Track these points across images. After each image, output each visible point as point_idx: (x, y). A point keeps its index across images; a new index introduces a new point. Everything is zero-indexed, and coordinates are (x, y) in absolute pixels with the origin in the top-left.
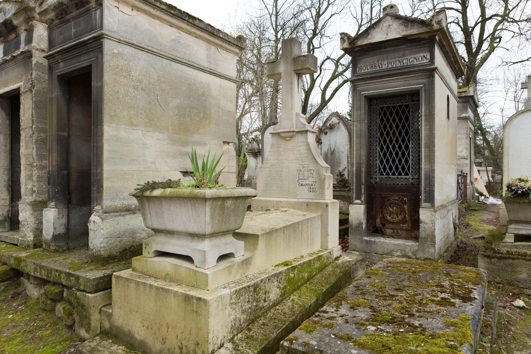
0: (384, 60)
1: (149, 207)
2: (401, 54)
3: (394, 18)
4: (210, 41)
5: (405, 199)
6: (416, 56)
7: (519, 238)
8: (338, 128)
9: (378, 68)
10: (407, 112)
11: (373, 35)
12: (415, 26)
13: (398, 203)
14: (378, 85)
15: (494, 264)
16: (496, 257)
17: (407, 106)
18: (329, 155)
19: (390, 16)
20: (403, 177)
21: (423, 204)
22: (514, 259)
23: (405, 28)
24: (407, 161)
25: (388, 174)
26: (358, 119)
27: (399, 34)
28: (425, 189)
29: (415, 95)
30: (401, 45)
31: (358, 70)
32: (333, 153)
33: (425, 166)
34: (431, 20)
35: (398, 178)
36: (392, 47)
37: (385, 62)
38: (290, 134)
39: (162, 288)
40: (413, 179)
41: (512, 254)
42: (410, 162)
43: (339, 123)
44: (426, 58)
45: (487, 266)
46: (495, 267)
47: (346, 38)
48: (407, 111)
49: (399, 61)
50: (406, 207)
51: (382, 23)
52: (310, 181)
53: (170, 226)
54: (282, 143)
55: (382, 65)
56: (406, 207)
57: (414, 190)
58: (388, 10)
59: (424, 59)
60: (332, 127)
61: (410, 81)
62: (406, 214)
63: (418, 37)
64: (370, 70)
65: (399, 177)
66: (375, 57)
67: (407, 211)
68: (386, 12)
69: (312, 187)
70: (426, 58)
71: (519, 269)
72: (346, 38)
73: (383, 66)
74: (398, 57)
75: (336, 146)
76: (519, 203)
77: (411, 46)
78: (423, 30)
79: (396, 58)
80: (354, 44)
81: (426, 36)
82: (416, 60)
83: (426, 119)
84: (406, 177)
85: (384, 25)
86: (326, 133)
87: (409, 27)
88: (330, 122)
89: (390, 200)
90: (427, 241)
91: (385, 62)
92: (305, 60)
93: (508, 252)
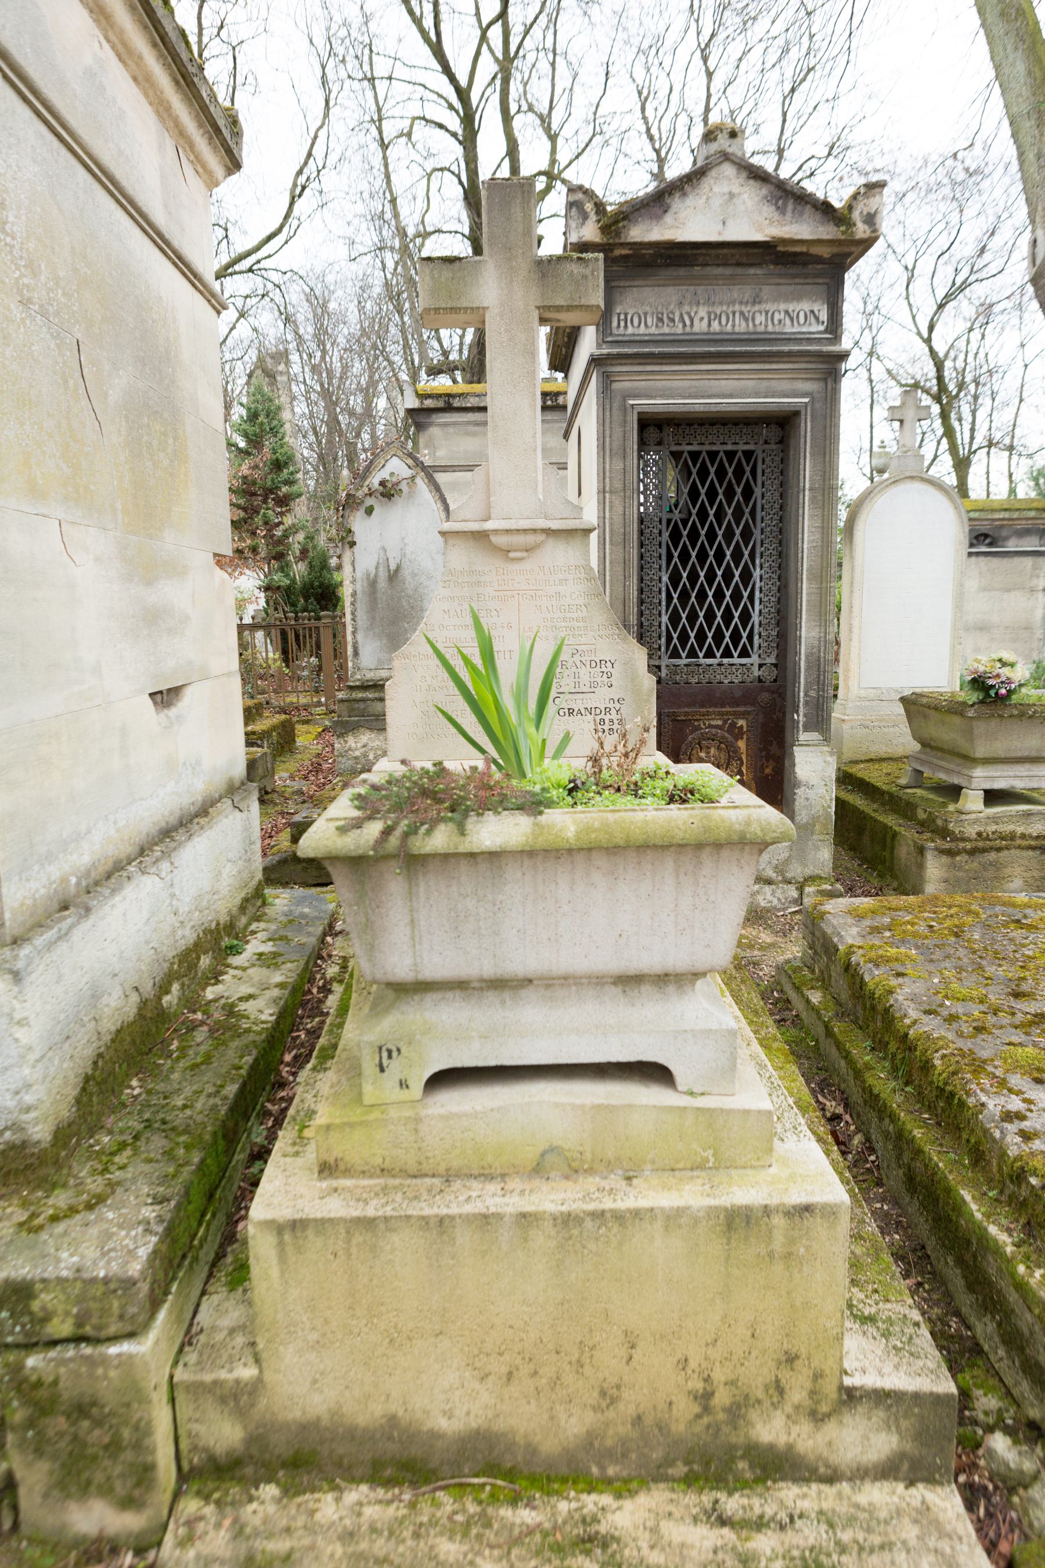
0: (698, 304)
1: (411, 895)
2: (748, 292)
3: (744, 175)
4: (168, 109)
5: (741, 722)
6: (791, 307)
7: (992, 797)
8: (411, 495)
9: (679, 329)
10: (748, 474)
11: (682, 215)
12: (806, 216)
13: (723, 737)
14: (686, 384)
15: (960, 869)
16: (965, 851)
17: (748, 455)
18: (382, 583)
19: (734, 162)
20: (736, 660)
21: (803, 736)
22: (999, 850)
23: (776, 216)
24: (745, 617)
25: (692, 654)
26: (619, 485)
27: (760, 229)
28: (806, 695)
29: (782, 424)
30: (751, 265)
31: (615, 324)
32: (394, 576)
33: (807, 632)
34: (850, 208)
35: (720, 665)
36: (725, 265)
37: (703, 312)
38: (531, 539)
39: (599, 1216)
40: (761, 666)
41: (987, 838)
42: (755, 618)
43: (413, 478)
44: (817, 319)
45: (946, 875)
46: (961, 874)
47: (589, 207)
48: (748, 469)
49: (742, 313)
50: (742, 744)
51: (707, 182)
52: (600, 699)
53: (520, 961)
54: (489, 567)
55: (692, 320)
56: (742, 744)
57: (765, 696)
58: (723, 142)
59: (813, 320)
60: (388, 492)
61: (773, 383)
62: (742, 764)
63: (804, 249)
64: (653, 330)
65: (725, 661)
66: (670, 290)
67: (744, 757)
68: (714, 147)
69: (607, 718)
70: (817, 319)
71: (1007, 871)
72: (589, 207)
73: (696, 321)
74: (741, 303)
75: (404, 555)
76: (1001, 716)
77: (780, 275)
78: (826, 232)
79: (733, 303)
80: (618, 234)
81: (825, 252)
82: (792, 319)
83: (813, 500)
84: (744, 661)
85: (716, 189)
86: (369, 511)
87: (789, 214)
88: (384, 474)
89: (699, 728)
90: (812, 833)
91: (703, 312)
92: (585, 277)
93: (979, 834)
